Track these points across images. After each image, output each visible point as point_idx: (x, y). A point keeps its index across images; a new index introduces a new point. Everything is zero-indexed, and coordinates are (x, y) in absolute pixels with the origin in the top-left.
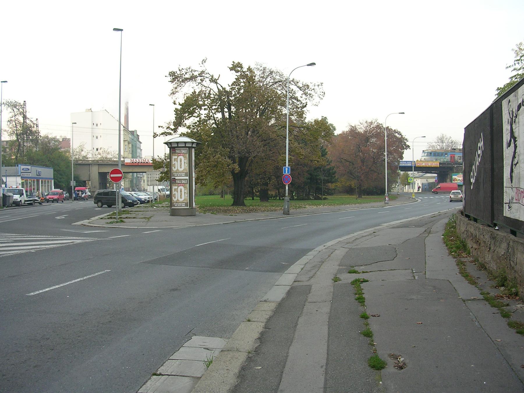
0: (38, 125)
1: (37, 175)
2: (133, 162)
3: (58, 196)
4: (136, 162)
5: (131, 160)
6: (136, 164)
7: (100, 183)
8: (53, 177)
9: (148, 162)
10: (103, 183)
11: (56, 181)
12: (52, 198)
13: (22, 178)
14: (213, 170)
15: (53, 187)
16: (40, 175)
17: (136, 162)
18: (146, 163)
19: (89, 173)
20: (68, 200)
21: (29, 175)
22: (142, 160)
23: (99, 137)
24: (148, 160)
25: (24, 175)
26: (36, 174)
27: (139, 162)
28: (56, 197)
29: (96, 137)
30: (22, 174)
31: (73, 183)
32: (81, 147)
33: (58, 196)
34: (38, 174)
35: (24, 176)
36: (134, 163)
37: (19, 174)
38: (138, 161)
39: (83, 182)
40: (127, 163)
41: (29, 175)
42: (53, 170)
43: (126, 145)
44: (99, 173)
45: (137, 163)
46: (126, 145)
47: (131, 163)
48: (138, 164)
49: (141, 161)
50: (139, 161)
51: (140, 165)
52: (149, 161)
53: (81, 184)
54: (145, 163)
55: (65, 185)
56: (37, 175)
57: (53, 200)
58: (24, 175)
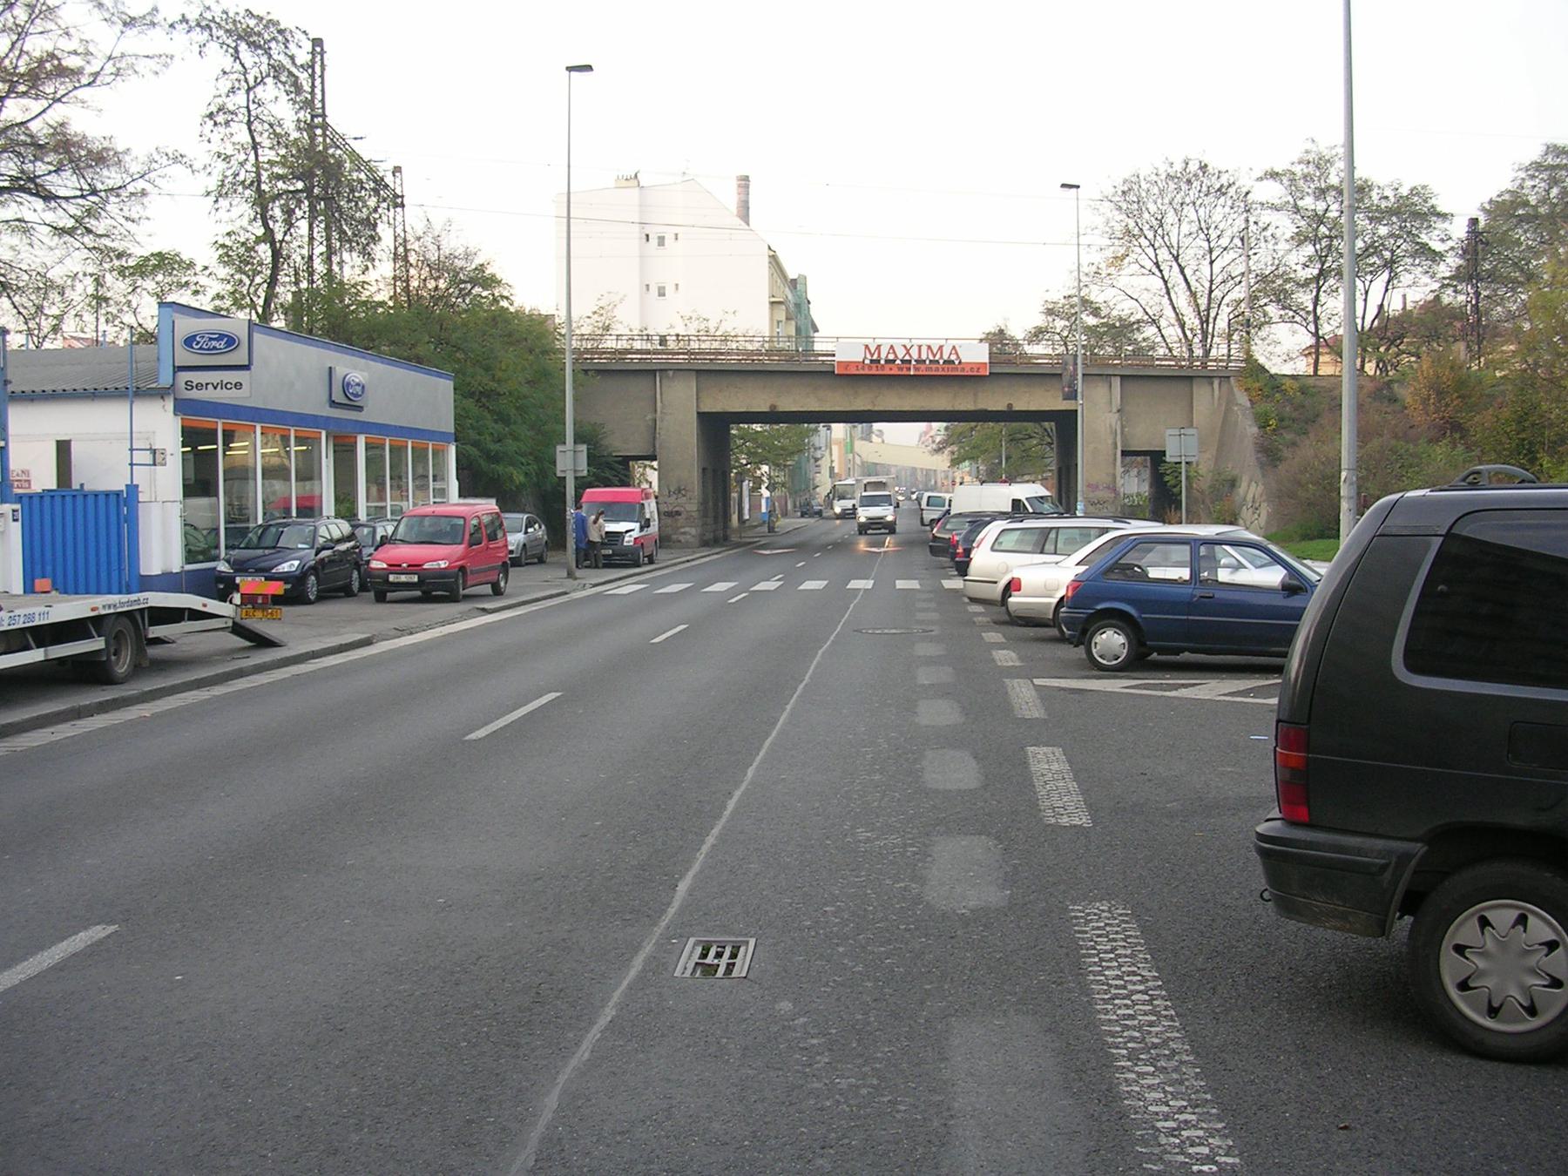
0: (402, 197)
1: (333, 404)
2: (878, 361)
3: (459, 549)
4: (891, 357)
5: (867, 347)
6: (895, 372)
7: (704, 469)
8: (450, 427)
9: (953, 357)
10: (714, 471)
11: (473, 451)
12: (414, 567)
13: (182, 407)
14: (1049, 440)
15: (454, 486)
16: (360, 409)
17: (894, 361)
18: (945, 362)
19: (649, 417)
20: (541, 561)
21: (238, 386)
22: (924, 350)
23: (669, 291)
24: (954, 348)
25: (199, 386)
26: (325, 397)
27: (907, 358)
28: (439, 558)
29: (659, 288)
30: (184, 377)
31: (570, 461)
32: (602, 315)
33: (459, 549)
34: (338, 397)
35: (195, 394)
36: (882, 362)
37: (165, 379)
38: (900, 357)
39: (619, 463)
40: (847, 364)
41: (238, 386)
42: (450, 384)
43: (778, 322)
44: (698, 413)
45: (898, 362)
46: (778, 322)
47: (867, 362)
48: (905, 372)
49: (915, 356)
50: (908, 352)
51: (912, 373)
52: (957, 353)
53: (608, 474)
54: (938, 362)
55: (522, 478)
56: (333, 404)
57: (415, 579)
58: (199, 386)
